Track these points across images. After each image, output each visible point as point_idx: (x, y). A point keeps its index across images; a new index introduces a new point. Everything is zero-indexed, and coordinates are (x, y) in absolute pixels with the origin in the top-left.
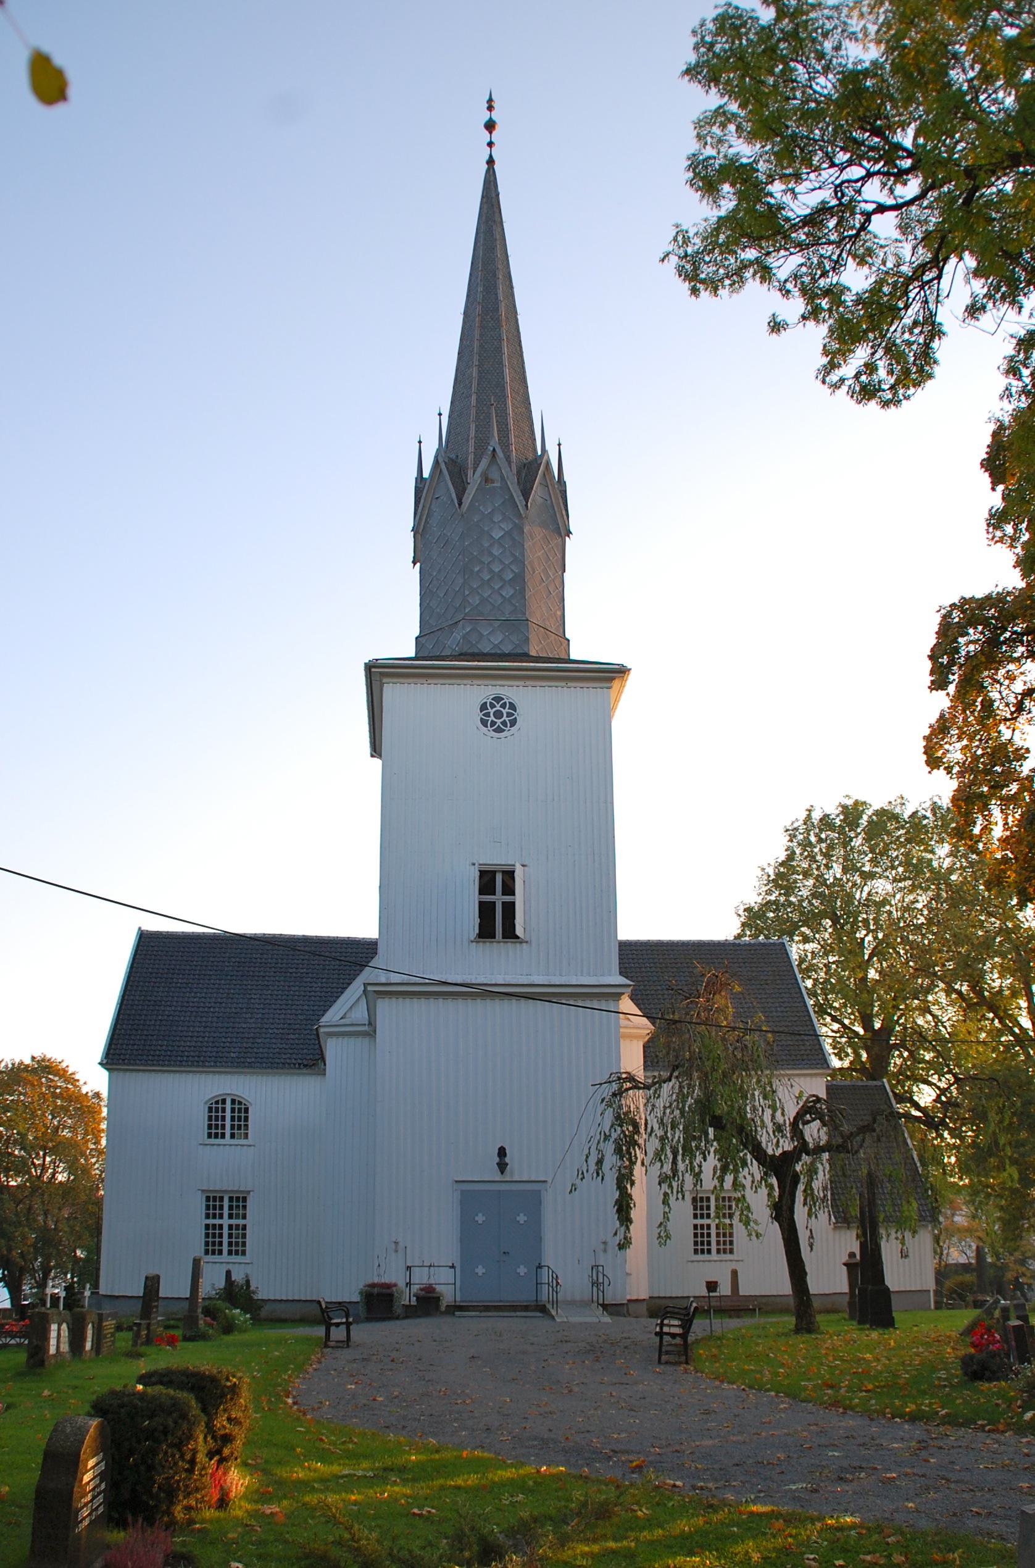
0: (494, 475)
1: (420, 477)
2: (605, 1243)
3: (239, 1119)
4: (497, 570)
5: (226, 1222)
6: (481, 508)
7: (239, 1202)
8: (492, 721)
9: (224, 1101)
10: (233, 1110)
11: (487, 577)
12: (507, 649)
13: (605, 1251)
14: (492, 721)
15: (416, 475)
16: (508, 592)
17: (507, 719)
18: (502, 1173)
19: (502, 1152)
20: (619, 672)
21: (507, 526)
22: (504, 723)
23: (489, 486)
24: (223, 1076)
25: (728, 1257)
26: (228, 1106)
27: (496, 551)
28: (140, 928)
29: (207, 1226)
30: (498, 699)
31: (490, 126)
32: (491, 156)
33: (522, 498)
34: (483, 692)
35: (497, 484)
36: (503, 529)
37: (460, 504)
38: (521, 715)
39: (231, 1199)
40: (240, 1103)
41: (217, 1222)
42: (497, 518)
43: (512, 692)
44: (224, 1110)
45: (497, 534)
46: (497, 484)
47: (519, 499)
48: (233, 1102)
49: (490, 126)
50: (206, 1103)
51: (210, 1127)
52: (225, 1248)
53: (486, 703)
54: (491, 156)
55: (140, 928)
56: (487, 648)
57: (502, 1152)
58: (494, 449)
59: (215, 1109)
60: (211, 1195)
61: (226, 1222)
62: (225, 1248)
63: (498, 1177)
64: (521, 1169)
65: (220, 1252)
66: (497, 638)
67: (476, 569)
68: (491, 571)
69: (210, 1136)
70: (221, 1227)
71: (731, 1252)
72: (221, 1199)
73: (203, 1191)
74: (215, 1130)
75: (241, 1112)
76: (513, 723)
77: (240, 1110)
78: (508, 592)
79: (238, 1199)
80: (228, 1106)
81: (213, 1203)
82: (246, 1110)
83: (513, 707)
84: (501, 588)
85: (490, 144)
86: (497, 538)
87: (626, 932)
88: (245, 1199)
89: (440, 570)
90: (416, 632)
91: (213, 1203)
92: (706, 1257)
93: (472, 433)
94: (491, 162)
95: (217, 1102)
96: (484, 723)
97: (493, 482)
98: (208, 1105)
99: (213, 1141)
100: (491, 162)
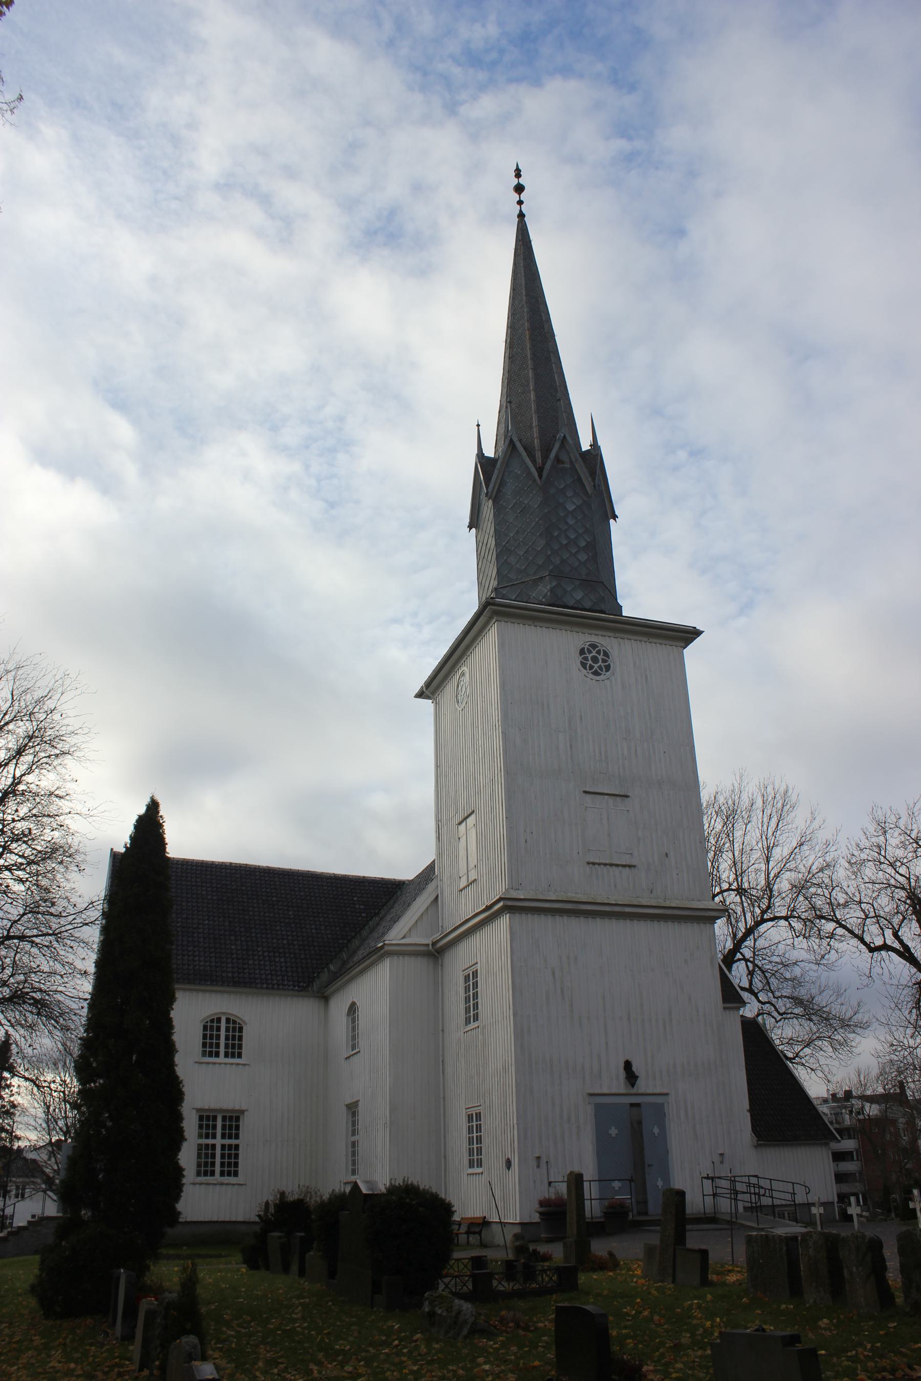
0: (564, 457)
1: (480, 455)
2: (722, 1155)
4: (572, 537)
5: (218, 1141)
6: (555, 483)
7: (478, 1116)
8: (590, 665)
9: (219, 1020)
10: (227, 1030)
11: (565, 542)
13: (722, 1162)
14: (590, 665)
15: (476, 452)
16: (583, 557)
17: (602, 664)
19: (628, 1065)
20: (688, 635)
21: (578, 502)
23: (561, 466)
25: (232, 1180)
28: (112, 849)
29: (200, 1146)
30: (594, 646)
31: (519, 189)
32: (521, 211)
33: (590, 479)
36: (575, 503)
39: (224, 1119)
40: (234, 1022)
41: (227, 1142)
42: (570, 493)
44: (219, 1029)
45: (571, 507)
46: (568, 466)
48: (228, 1020)
49: (519, 189)
50: (201, 1021)
52: (218, 1169)
53: (584, 648)
54: (521, 211)
55: (112, 849)
57: (628, 1065)
58: (565, 437)
60: (228, 1115)
62: (218, 1169)
66: (579, 595)
67: (556, 534)
68: (567, 537)
69: (204, 1054)
71: (236, 1174)
72: (215, 1118)
73: (198, 1110)
75: (236, 1029)
77: (234, 1029)
78: (583, 557)
79: (231, 1118)
81: (349, 1107)
82: (241, 1029)
84: (577, 552)
85: (520, 203)
86: (571, 510)
88: (238, 1119)
89: (518, 531)
92: (209, 1179)
93: (535, 423)
94: (521, 215)
95: (212, 1021)
97: (563, 463)
98: (203, 1023)
100: (521, 215)
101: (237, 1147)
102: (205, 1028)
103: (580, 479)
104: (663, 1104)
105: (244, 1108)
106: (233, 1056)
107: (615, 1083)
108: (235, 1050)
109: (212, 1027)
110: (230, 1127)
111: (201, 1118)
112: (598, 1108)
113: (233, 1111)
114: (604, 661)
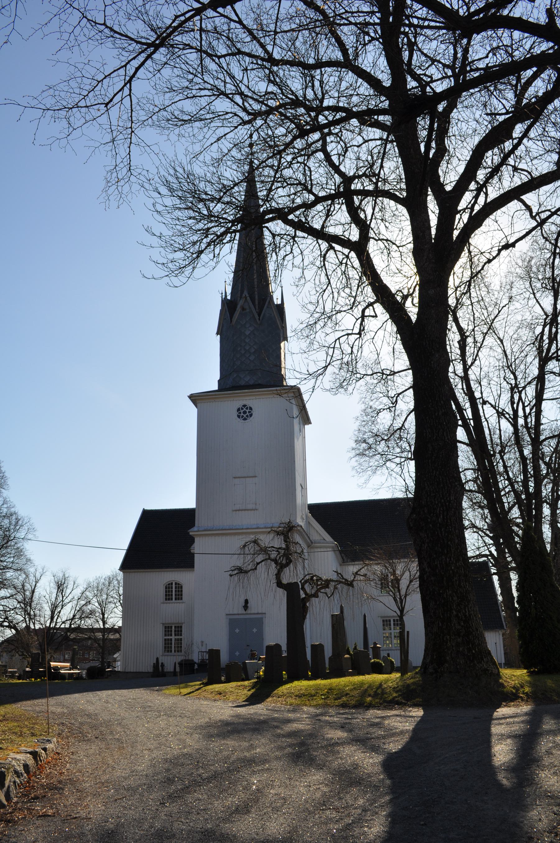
3: (169, 591)
4: (248, 348)
5: (173, 637)
9: (172, 584)
12: (251, 382)
18: (245, 610)
19: (246, 601)
21: (251, 329)
22: (247, 416)
24: (174, 573)
26: (174, 586)
27: (247, 340)
29: (165, 640)
30: (244, 406)
34: (239, 403)
35: (248, 311)
37: (231, 321)
38: (254, 412)
39: (175, 627)
40: (179, 584)
41: (170, 637)
43: (249, 402)
44: (172, 588)
45: (247, 333)
47: (257, 316)
48: (176, 584)
51: (166, 595)
56: (242, 383)
57: (246, 601)
59: (168, 587)
60: (385, 619)
61: (173, 637)
63: (244, 612)
64: (254, 608)
65: (171, 651)
66: (247, 379)
67: (239, 349)
69: (166, 599)
70: (171, 639)
72: (171, 627)
74: (168, 597)
75: (179, 587)
76: (251, 415)
80: (174, 586)
82: (182, 587)
83: (251, 408)
87: (312, 500)
88: (181, 627)
90: (219, 378)
91: (167, 629)
95: (169, 584)
96: (239, 416)
99: (168, 601)
101: (181, 639)
102: (166, 588)
103: (254, 316)
104: (262, 618)
105: (183, 622)
106: (179, 599)
107: (238, 609)
108: (179, 596)
109: (169, 587)
110: (168, 631)
111: (165, 627)
112: (230, 620)
113: (178, 623)
114: (243, 416)
